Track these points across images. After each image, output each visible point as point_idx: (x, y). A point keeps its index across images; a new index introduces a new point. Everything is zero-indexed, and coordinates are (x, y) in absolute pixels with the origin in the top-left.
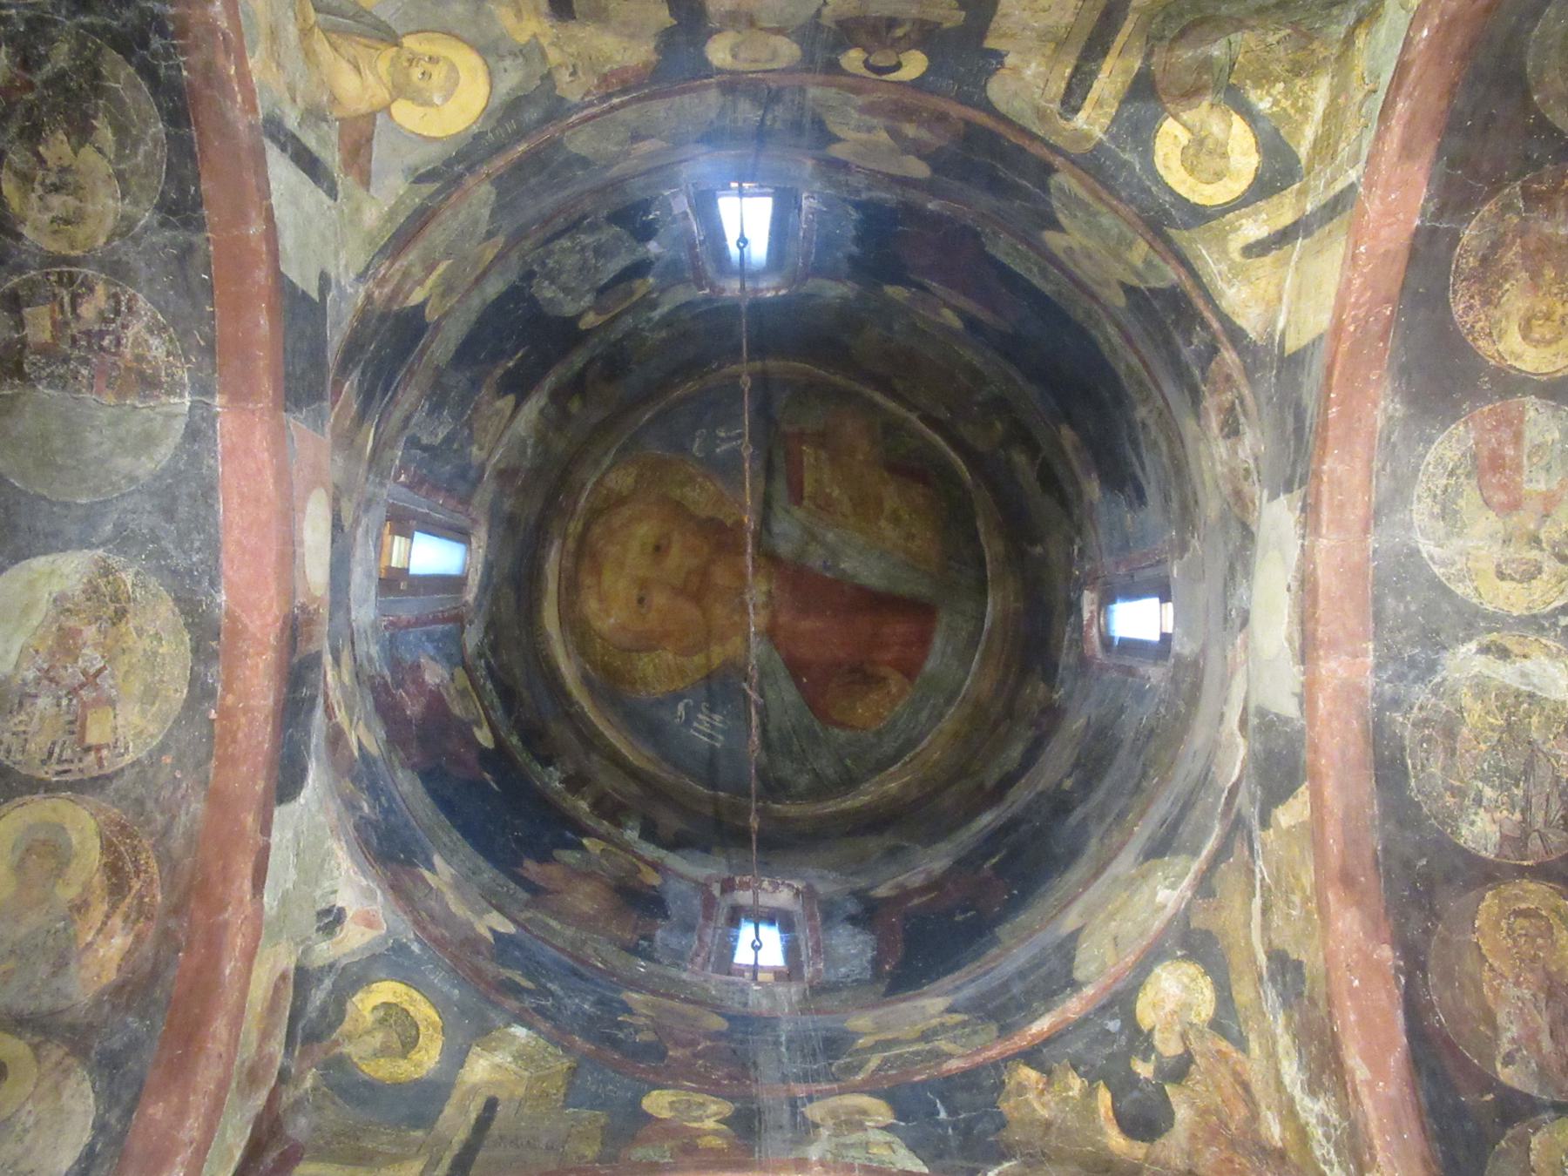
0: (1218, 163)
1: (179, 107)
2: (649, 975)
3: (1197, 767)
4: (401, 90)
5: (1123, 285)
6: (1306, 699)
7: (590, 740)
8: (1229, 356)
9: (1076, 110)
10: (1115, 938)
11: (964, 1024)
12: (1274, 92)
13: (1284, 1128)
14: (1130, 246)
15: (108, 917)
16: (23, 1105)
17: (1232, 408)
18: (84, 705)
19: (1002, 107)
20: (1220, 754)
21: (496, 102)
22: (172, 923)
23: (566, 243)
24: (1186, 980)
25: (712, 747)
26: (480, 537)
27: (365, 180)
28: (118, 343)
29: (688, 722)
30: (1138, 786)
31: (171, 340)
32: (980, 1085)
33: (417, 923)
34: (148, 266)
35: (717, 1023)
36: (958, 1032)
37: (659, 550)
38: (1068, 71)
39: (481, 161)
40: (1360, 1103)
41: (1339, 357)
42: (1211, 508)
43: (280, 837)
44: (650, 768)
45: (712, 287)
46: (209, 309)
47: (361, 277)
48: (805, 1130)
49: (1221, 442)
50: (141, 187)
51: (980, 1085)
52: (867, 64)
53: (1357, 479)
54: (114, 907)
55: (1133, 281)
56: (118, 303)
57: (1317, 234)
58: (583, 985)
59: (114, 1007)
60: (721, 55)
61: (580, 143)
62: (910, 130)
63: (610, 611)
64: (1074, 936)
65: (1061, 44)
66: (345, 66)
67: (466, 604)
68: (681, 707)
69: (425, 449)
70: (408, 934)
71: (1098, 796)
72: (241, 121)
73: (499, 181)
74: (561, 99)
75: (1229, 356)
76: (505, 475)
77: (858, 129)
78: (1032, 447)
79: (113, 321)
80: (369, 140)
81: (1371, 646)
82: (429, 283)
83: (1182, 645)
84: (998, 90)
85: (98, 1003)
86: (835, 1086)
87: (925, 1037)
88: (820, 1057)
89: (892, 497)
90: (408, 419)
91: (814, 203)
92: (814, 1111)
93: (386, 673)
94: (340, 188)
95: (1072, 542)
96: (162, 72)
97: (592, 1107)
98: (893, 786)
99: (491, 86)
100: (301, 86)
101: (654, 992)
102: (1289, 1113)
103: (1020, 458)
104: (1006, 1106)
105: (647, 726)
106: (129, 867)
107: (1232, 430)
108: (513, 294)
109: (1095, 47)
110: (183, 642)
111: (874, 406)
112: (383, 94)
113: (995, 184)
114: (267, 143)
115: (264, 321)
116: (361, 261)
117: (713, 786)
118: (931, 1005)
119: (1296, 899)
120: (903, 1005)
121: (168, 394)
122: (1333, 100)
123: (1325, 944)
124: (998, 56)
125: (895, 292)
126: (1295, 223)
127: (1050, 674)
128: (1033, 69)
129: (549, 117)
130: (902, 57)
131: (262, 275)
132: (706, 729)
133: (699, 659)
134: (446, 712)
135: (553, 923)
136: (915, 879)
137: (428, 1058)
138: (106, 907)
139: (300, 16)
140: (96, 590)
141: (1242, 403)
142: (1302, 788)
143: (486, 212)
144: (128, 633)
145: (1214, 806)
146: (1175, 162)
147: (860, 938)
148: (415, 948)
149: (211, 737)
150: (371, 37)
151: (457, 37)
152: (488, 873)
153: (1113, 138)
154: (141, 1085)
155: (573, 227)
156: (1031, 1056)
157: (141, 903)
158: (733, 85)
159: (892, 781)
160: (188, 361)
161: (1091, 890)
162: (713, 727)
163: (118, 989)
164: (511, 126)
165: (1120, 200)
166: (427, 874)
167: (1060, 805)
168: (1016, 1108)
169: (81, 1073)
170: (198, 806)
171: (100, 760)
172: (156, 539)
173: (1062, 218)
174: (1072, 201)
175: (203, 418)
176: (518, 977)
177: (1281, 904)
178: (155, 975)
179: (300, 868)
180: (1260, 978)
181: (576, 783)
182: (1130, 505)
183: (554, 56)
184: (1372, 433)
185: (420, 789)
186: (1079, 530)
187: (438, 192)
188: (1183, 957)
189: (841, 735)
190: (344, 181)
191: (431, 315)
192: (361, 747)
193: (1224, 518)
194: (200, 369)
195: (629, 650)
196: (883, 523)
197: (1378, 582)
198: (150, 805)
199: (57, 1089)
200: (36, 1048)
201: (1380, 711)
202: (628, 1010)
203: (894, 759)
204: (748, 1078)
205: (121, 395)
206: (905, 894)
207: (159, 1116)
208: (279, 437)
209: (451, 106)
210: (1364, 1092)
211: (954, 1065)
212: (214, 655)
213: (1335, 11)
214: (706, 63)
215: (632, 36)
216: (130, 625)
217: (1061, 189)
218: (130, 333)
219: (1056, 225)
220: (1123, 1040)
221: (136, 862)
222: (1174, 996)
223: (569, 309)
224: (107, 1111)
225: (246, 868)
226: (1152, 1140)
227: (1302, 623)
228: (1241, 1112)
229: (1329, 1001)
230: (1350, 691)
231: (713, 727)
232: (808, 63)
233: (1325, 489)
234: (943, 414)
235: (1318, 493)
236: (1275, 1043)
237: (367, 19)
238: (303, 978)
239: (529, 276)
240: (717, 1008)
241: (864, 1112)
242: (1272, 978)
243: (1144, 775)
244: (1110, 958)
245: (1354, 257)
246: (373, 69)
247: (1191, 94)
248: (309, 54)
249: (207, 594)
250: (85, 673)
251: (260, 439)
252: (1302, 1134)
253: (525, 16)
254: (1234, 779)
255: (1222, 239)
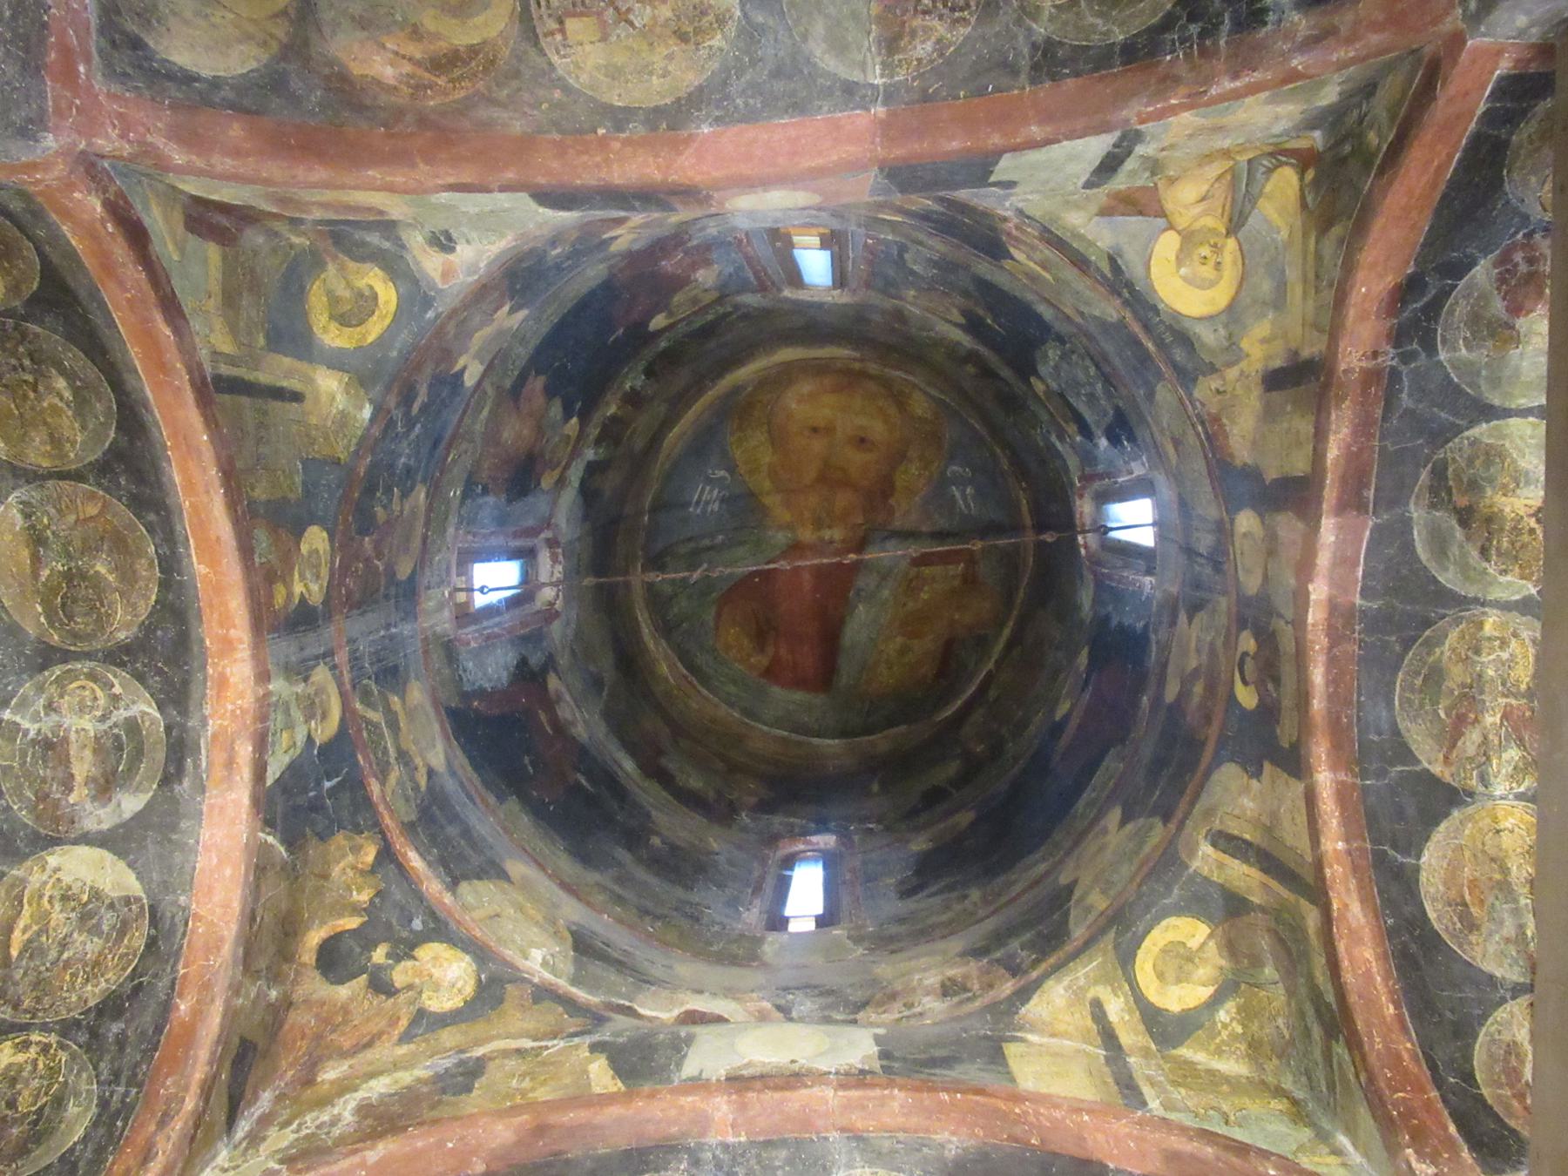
0: (1171, 975)
1: (1138, 54)
2: (448, 502)
3: (657, 972)
4: (1189, 239)
5: (1075, 882)
6: (698, 1085)
7: (680, 403)
8: (1008, 987)
9: (1214, 845)
10: (498, 915)
11: (416, 788)
12: (1234, 1024)
13: (332, 1082)
14: (1103, 892)
15: (410, 59)
16: (231, 10)
17: (966, 990)
18: (599, 14)
19: (1215, 777)
20: (665, 993)
21: (1187, 324)
22: (409, 118)
23: (1092, 370)
24: (460, 984)
25: (688, 504)
26: (842, 298)
27: (1106, 212)
28: (925, 12)
29: (709, 481)
30: (647, 912)
31: (932, 61)
32: (357, 812)
33: (454, 312)
34: (997, 35)
35: (404, 570)
36: (409, 785)
37: (862, 442)
38: (1247, 837)
39: (1135, 312)
40: (347, 1156)
41: (993, 1100)
42: (885, 969)
43: (503, 200)
44: (662, 457)
45: (1084, 488)
46: (962, 94)
47: (1020, 212)
48: (299, 671)
49: (939, 978)
50: (1066, 23)
51: (357, 812)
52: (1245, 654)
53: (887, 1120)
54: (418, 63)
55: (1077, 894)
56: (962, 10)
57: (1106, 1070)
58: (424, 451)
59: (328, 78)
60: (1245, 523)
61: (1165, 394)
62: (1198, 689)
63: (804, 404)
64: (503, 875)
65: (1269, 830)
66: (1205, 187)
67: (780, 290)
68: (722, 473)
69: (901, 256)
70: (441, 307)
71: (641, 874)
72: (1131, 112)
73: (1121, 325)
74: (1195, 380)
75: (1008, 987)
76: (899, 315)
77: (1199, 640)
78: (964, 779)
79: (945, 6)
80: (1141, 213)
81: (743, 1139)
82: (1031, 264)
83: (772, 943)
84: (1229, 775)
85: (330, 63)
86: (348, 687)
87: (403, 756)
88: (375, 668)
89: (927, 644)
90: (920, 243)
91: (1147, 589)
92: (321, 674)
93: (695, 242)
94: (1095, 190)
95: (879, 822)
96: (1168, 36)
97: (304, 483)
98: (664, 669)
99: (1200, 319)
100: (1177, 154)
101: (430, 509)
102: (344, 1087)
103: (952, 768)
104: (340, 839)
105: (704, 444)
106: (457, 73)
107: (948, 989)
108: (1045, 328)
109: (1269, 861)
110: (663, 97)
111: (1002, 625)
112: (1182, 222)
113: (1159, 764)
114: (1117, 134)
115: (955, 145)
116: (1037, 213)
117: (654, 510)
118: (436, 752)
119: (526, 1084)
120: (437, 727)
121: (883, 63)
122: (1227, 1079)
123: (484, 1114)
124: (1257, 774)
125: (1083, 659)
126: (1120, 1047)
127: (764, 808)
128: (1248, 804)
129: (1179, 370)
130: (1252, 687)
131: (996, 140)
132: (706, 497)
133: (767, 484)
134: (675, 291)
135: (485, 412)
136: (565, 711)
137: (333, 337)
138: (418, 56)
139: (1242, 149)
140: (704, 13)
141: (968, 999)
142: (620, 1084)
143: (1097, 313)
144: (667, 46)
145: (620, 995)
146: (1171, 936)
147: (505, 674)
148: (430, 314)
149: (581, 132)
150: (1232, 206)
151: (1240, 285)
152: (523, 353)
153: (1192, 878)
154: (257, 113)
155: (1107, 380)
156: (387, 855)
157: (426, 87)
158: (1223, 531)
159: (669, 666)
160: (914, 79)
161: (547, 882)
162: (707, 503)
163: (344, 78)
164: (1168, 339)
165: (1140, 886)
166: (506, 308)
167: (635, 838)
168: (339, 848)
169: (265, 57)
170: (518, 127)
171: (552, 33)
172: (753, 63)
173: (1129, 827)
174: (1140, 838)
175: (864, 96)
176: (422, 397)
177: (523, 1068)
178: (360, 108)
179: (480, 216)
180: (462, 1051)
181: (634, 400)
182: (902, 882)
183: (1232, 373)
184: (927, 1131)
185: (593, 284)
186: (888, 829)
187: (1104, 276)
188: (480, 980)
189: (709, 616)
190: (1101, 194)
191: (1007, 264)
192: (616, 238)
193: (874, 982)
194: (907, 91)
195: (769, 423)
196: (899, 640)
197: (799, 1143)
198: (515, 84)
199: (249, 37)
200: (284, 13)
201: (688, 1150)
202: (405, 495)
203: (692, 668)
204: (351, 608)
205: (880, 20)
206: (549, 704)
207: (232, 133)
208: (855, 166)
209: (1179, 283)
210: (355, 1159)
211: (375, 788)
212: (654, 128)
213: (1304, 1079)
214: (1239, 509)
215: (1254, 443)
216: (675, 47)
217: (1151, 828)
218: (936, 23)
219: (1124, 822)
220: (405, 934)
221: (461, 78)
222: (446, 975)
223: (1043, 370)
224: (232, 87)
225: (466, 178)
226: (318, 967)
227: (762, 1076)
228: (347, 1044)
229: (435, 1122)
230: (703, 1122)
231: (707, 503)
232: (1244, 602)
233: (877, 1092)
234: (992, 694)
235: (872, 1086)
236: (405, 1068)
237: (1248, 206)
238: (388, 227)
239: (1061, 340)
240: (423, 560)
241: (324, 716)
242: (461, 1063)
243: (657, 917)
244: (477, 914)
245: (1079, 1111)
246: (1205, 213)
247: (1231, 948)
248: (1208, 158)
249: (708, 116)
250: (629, 10)
251: (850, 151)
252: (324, 1102)
253: (1265, 347)
254: (641, 1011)
255: (1105, 978)
